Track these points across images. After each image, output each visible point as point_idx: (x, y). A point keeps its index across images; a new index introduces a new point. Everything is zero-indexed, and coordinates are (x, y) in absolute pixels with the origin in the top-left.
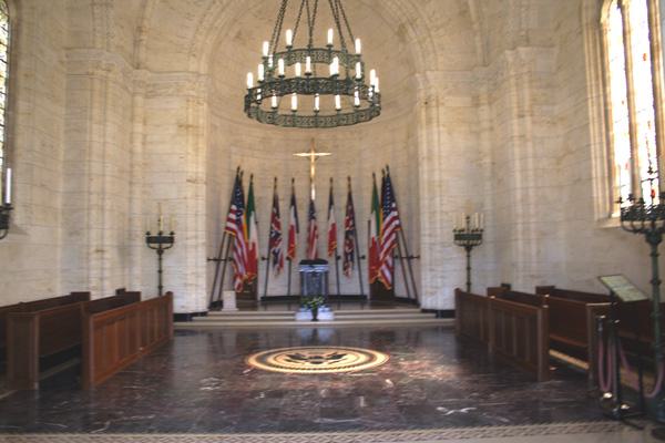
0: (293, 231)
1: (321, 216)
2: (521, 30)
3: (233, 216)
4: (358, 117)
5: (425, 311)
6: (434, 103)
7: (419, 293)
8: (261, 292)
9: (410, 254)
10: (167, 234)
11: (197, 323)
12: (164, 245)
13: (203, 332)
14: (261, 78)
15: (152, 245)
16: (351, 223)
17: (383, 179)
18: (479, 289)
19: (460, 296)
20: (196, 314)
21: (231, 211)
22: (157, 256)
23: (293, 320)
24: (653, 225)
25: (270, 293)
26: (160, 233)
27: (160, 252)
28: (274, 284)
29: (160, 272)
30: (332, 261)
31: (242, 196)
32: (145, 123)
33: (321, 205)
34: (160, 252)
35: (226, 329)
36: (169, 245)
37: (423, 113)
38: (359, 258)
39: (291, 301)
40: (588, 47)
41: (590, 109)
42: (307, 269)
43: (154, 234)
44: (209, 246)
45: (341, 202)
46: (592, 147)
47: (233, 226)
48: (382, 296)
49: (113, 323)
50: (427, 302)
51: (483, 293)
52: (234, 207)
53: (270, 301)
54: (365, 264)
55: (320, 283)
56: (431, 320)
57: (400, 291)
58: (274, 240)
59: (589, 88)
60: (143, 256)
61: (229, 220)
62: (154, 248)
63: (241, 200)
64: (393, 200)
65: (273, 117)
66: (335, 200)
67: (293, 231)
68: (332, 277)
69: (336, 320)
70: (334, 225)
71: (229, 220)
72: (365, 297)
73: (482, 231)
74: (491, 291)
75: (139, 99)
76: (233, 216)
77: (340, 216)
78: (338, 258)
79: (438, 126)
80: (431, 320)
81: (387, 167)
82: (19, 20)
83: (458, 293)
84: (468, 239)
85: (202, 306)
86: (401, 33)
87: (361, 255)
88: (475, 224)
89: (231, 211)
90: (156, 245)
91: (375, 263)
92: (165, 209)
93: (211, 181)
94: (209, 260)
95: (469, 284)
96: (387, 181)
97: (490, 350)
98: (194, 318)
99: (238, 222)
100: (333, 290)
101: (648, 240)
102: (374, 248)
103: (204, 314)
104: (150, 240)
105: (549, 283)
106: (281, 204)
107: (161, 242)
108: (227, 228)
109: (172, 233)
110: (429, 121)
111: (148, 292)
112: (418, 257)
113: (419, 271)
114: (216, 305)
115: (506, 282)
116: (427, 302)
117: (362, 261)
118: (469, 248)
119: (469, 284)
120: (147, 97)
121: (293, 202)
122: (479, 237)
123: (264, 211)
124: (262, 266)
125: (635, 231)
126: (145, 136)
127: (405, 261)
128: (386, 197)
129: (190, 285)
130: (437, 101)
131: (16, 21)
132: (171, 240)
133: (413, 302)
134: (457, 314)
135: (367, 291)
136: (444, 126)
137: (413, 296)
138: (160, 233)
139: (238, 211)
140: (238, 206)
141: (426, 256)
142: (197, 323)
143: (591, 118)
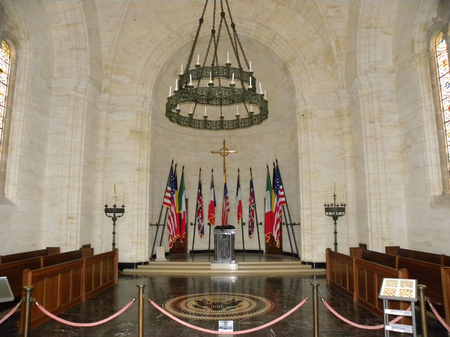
0: (213, 205)
1: (232, 195)
2: (369, 62)
3: (169, 195)
4: (252, 120)
5: (304, 263)
6: (309, 115)
7: (299, 251)
8: (190, 248)
9: (138, 172)
10: (119, 207)
11: (141, 270)
12: (117, 215)
13: (145, 277)
14: (177, 89)
15: (108, 214)
16: (252, 201)
17: (274, 169)
18: (344, 250)
19: (331, 254)
20: (140, 264)
21: (167, 191)
22: (112, 222)
23: (209, 269)
24: (335, 214)
25: (196, 248)
26: (115, 206)
27: (114, 219)
28: (198, 242)
29: (114, 233)
30: (238, 226)
31: (176, 180)
32: (108, 130)
33: (232, 187)
34: (114, 219)
35: (160, 275)
36: (121, 214)
37: (301, 122)
38: (257, 225)
39: (209, 254)
40: (421, 71)
41: (424, 114)
42: (220, 233)
43: (111, 206)
44: (152, 215)
45: (245, 186)
46: (428, 142)
47: (169, 202)
48: (274, 251)
49: (57, 274)
50: (305, 256)
51: (347, 252)
52: (169, 189)
53: (195, 253)
54: (262, 229)
55: (229, 243)
56: (308, 270)
57: (286, 248)
58: (199, 211)
59: (423, 99)
60: (103, 222)
61: (166, 197)
62: (110, 216)
63: (174, 183)
64: (281, 184)
65: (190, 122)
66: (242, 184)
67: (213, 205)
68: (238, 238)
69: (239, 269)
70: (240, 202)
71: (166, 197)
72: (263, 251)
73: (345, 205)
74: (352, 250)
75: (104, 113)
76: (169, 195)
77: (245, 195)
78: (243, 224)
79: (312, 131)
80: (308, 270)
81: (277, 161)
82: (17, 58)
83: (329, 250)
84: (335, 211)
85: (144, 257)
86: (285, 69)
87: (259, 222)
88: (340, 201)
89: (167, 191)
90: (112, 215)
91: (268, 228)
92: (119, 189)
93: (153, 171)
94: (151, 225)
95: (336, 244)
96: (277, 172)
97: (355, 300)
98: (138, 266)
99: (172, 199)
100: (238, 246)
101: (333, 219)
102: (269, 217)
103: (146, 263)
104: (107, 210)
105: (395, 244)
106: (203, 187)
107: (115, 212)
108: (164, 203)
109: (123, 206)
110: (306, 128)
111: (100, 247)
112: (299, 224)
113: (300, 234)
114: (154, 257)
115: (363, 242)
116: (305, 256)
117: (259, 226)
118: (335, 218)
119: (336, 244)
120: (109, 112)
121: (212, 186)
122: (343, 210)
123: (191, 193)
124: (191, 229)
125: (329, 216)
126: (108, 139)
127: (289, 226)
128: (275, 182)
129: (134, 243)
130: (311, 114)
131: (15, 58)
132: (122, 211)
133: (295, 256)
134: (328, 265)
135: (263, 247)
136: (316, 131)
137: (295, 251)
138: (115, 206)
139: (171, 191)
140: (172, 188)
141: (305, 224)
142: (141, 270)
143: (425, 121)
